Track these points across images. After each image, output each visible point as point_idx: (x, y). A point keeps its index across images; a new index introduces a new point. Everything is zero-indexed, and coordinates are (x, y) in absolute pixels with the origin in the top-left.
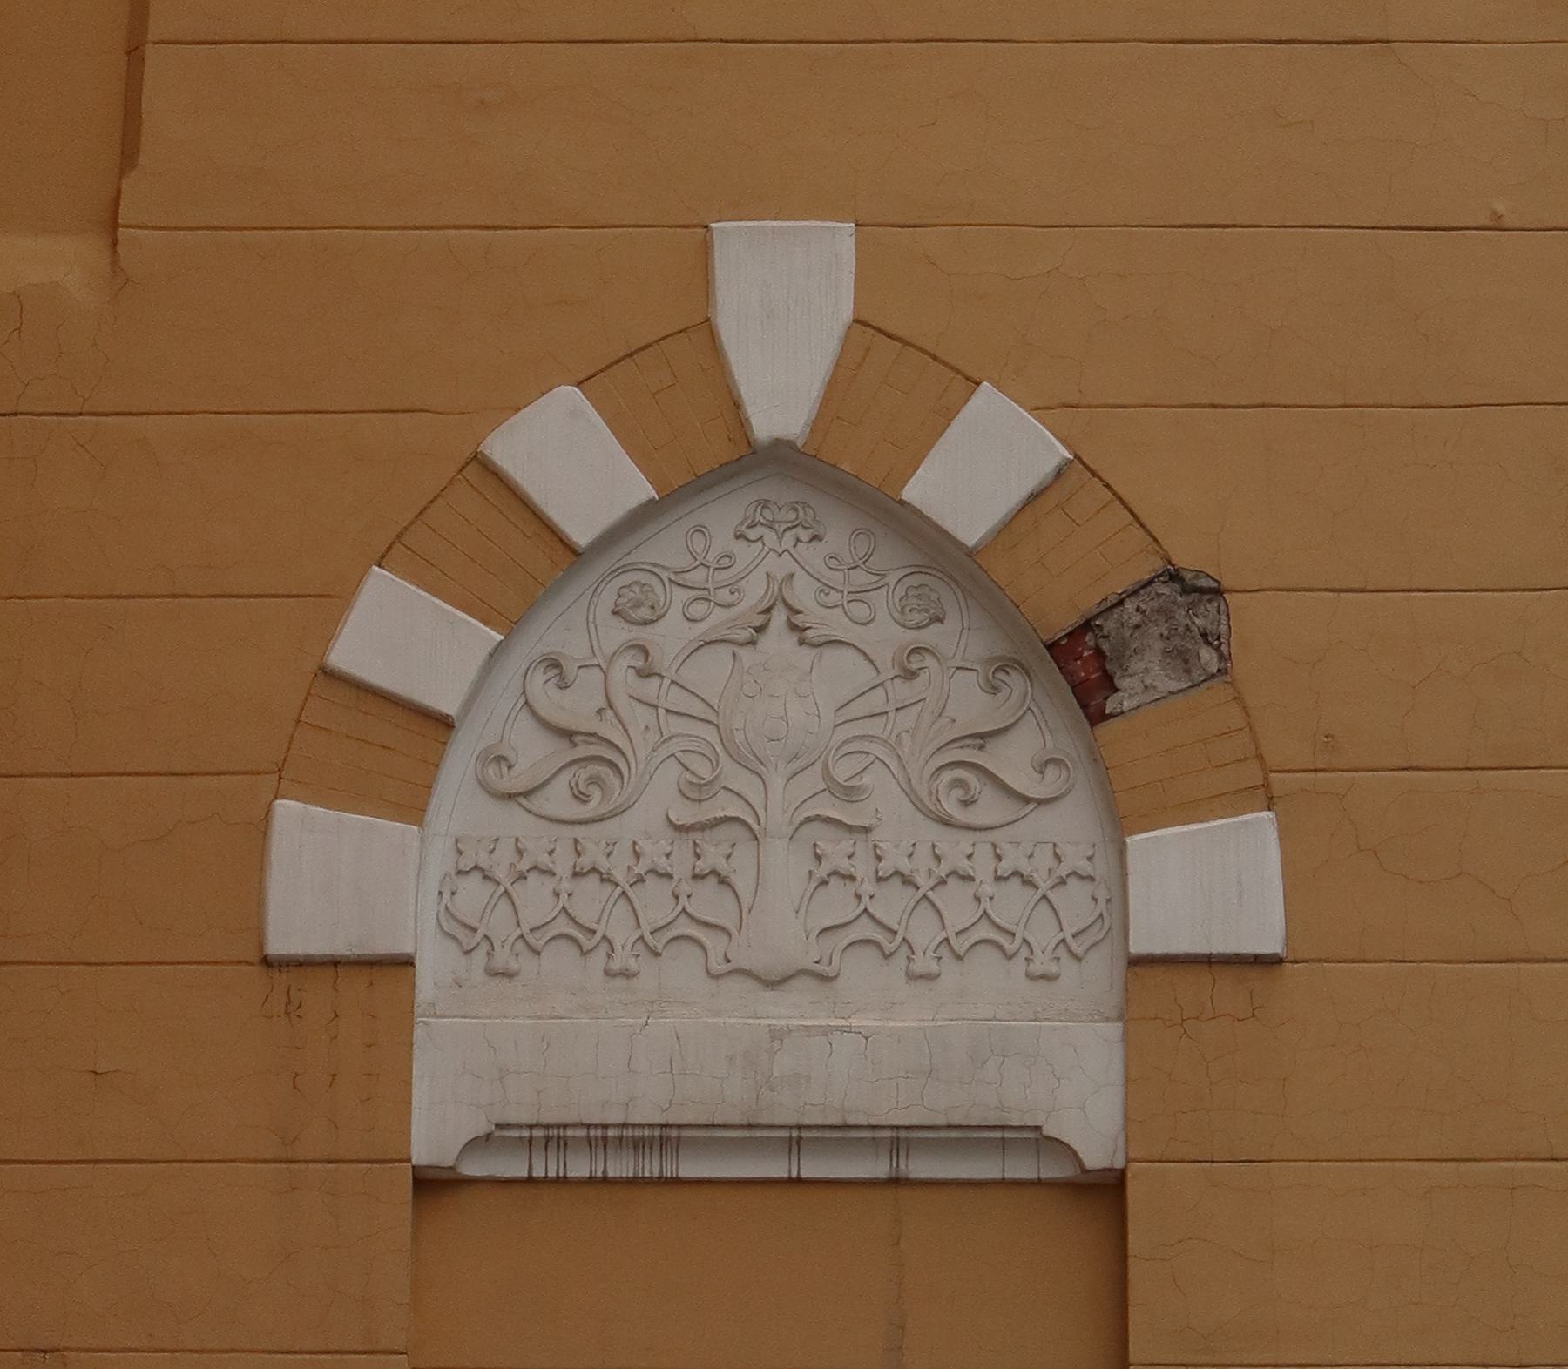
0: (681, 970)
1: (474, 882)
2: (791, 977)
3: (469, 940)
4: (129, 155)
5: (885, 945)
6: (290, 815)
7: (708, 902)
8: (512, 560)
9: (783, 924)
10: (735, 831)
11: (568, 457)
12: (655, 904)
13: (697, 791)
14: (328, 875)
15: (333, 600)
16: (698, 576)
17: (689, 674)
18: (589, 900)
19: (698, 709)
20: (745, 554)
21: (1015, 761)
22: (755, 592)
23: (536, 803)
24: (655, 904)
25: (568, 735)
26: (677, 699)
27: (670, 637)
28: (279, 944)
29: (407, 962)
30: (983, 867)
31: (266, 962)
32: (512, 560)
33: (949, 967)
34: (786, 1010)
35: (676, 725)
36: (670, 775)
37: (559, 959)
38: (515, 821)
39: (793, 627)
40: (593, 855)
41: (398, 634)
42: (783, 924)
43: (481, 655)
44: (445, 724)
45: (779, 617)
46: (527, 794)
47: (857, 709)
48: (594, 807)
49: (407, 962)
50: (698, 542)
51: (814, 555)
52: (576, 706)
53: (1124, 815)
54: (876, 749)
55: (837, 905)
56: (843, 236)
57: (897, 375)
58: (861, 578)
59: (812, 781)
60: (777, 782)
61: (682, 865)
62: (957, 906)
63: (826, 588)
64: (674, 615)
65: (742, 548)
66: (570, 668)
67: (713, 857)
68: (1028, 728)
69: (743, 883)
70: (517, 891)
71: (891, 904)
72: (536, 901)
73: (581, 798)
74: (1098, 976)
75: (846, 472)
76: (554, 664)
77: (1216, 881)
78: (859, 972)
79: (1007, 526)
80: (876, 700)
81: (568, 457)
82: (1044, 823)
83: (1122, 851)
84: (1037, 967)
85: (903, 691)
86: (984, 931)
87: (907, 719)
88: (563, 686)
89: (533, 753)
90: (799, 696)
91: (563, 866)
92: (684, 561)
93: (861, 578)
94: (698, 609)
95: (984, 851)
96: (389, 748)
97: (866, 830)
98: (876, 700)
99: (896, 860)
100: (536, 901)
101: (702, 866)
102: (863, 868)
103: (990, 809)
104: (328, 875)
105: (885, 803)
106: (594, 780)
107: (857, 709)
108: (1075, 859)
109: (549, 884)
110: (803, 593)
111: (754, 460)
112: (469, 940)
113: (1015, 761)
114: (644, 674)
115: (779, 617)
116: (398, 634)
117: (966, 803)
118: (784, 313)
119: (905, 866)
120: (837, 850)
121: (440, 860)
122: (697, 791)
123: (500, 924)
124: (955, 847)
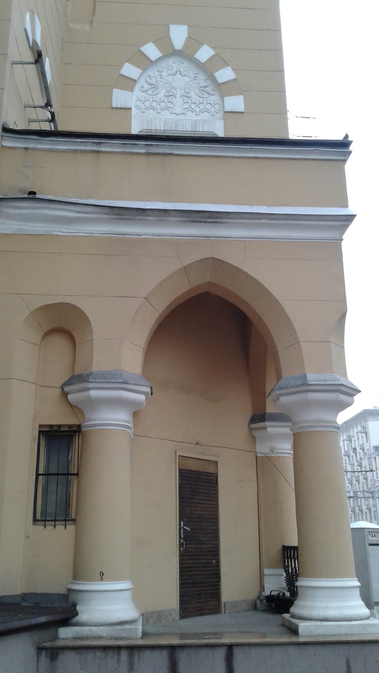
0: (166, 112)
1: (139, 101)
2: (49, 458)
3: (139, 108)
4: (94, 14)
5: (192, 110)
6: (115, 90)
7: (170, 105)
8: (145, 63)
9: (178, 110)
10: (173, 97)
11: (151, 51)
12: (163, 105)
13: (168, 92)
14: (120, 98)
15: (121, 66)
16: (168, 67)
17: (166, 79)
18: (154, 104)
19: (167, 82)
20: (174, 65)
21: (209, 89)
22: (175, 69)
23: (147, 92)
24: (163, 105)
25: (151, 85)
26: (165, 81)
27: (164, 74)
28: (114, 106)
29: (130, 109)
30: (205, 102)
31: (112, 108)
32: (145, 63)
33: (201, 114)
34: (181, 117)
35: (165, 84)
36: (165, 90)
37: (151, 111)
38: (144, 94)
39: (180, 73)
40: (155, 99)
41: (129, 70)
42: (178, 110)
43: (140, 73)
44: (135, 81)
45: (178, 72)
46: (147, 91)
47: (188, 83)
48: (155, 93)
49: (130, 109)
50: (168, 63)
51: (183, 65)
52: (153, 81)
53: (222, 97)
54: (191, 88)
55: (186, 106)
56: (186, 27)
57: (193, 42)
58: (188, 69)
59: (183, 91)
60: (178, 91)
61: (166, 100)
62: (202, 106)
63: (184, 69)
64: (165, 71)
65: (173, 64)
66: (152, 77)
67: (170, 100)
68: (210, 86)
69: (174, 102)
70: (145, 103)
71: (193, 106)
72: (147, 104)
73: (153, 92)
74: (220, 115)
75: (186, 54)
76: (149, 76)
77: (236, 103)
78: (189, 113)
79: (208, 60)
80: (191, 83)
81: (151, 51)
82: (212, 98)
83: (223, 101)
84: (212, 114)
85: (195, 82)
86: (205, 110)
87: (195, 85)
88: (151, 79)
89: (147, 87)
90: (180, 82)
91: (151, 100)
92: (166, 65)
93: (188, 69)
94: (168, 71)
95: (205, 101)
96: (129, 84)
97: (190, 97)
98: (191, 83)
99: (194, 101)
100: (147, 104)
101: (169, 101)
102: (190, 102)
103: (206, 95)
104: (120, 98)
105: (192, 93)
106: (155, 90)
107: (188, 83)
108: (217, 102)
109: (149, 102)
110: (181, 69)
111: (175, 53)
112: (139, 108)
113: (209, 89)
114: (161, 78)
115: (178, 72)
116: (129, 70)
117: (203, 95)
118: (179, 35)
119: (195, 102)
120: (186, 100)
121: (134, 99)
122: (168, 92)
123: (143, 106)
124: (201, 100)
